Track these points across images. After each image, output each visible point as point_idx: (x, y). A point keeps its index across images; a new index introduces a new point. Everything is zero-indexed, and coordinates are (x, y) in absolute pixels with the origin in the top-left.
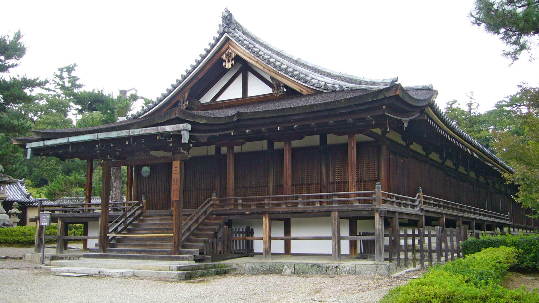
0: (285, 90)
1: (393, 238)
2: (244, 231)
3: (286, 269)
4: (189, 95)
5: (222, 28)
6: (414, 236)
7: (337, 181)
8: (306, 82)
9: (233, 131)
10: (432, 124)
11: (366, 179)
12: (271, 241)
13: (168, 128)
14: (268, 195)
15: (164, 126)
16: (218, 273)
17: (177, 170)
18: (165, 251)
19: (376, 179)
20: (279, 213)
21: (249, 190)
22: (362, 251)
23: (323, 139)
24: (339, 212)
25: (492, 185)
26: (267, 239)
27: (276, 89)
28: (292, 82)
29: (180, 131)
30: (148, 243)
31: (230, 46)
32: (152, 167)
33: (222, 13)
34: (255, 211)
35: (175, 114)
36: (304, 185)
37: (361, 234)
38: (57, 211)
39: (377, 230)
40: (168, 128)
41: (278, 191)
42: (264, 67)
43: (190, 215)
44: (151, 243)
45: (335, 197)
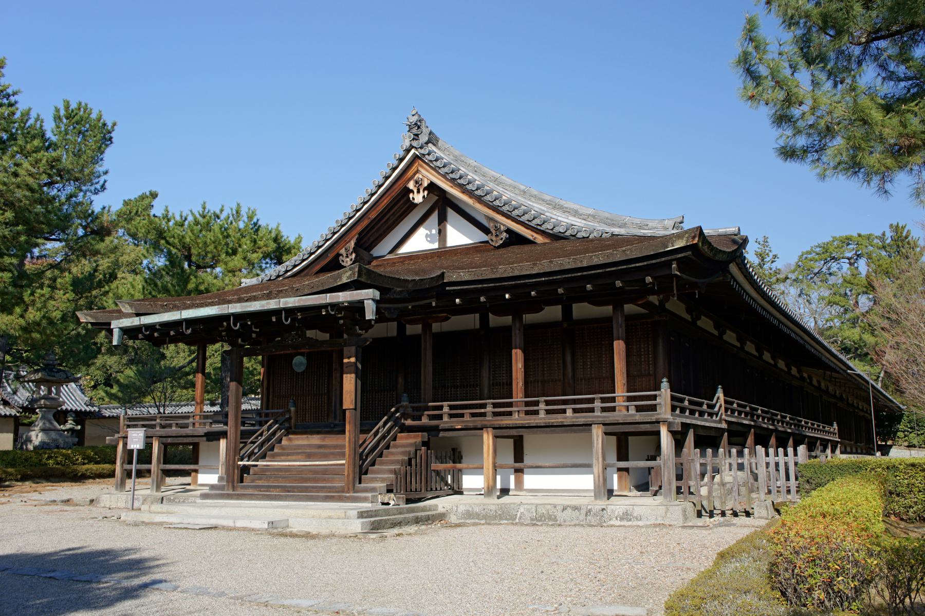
4: (355, 244)
9: (434, 299)
15: (336, 294)
16: (417, 521)
21: (451, 391)
23: (567, 312)
25: (808, 381)
27: (494, 234)
31: (420, 169)
32: (309, 356)
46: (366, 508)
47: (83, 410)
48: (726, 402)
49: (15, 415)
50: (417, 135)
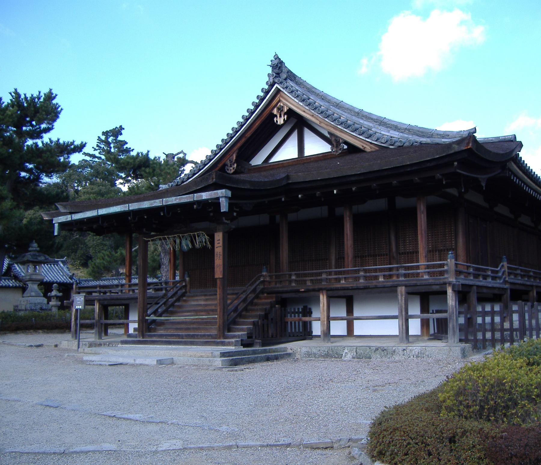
0: (346, 147)
1: (469, 316)
2: (300, 310)
3: (346, 353)
4: (237, 157)
5: (271, 78)
6: (493, 313)
7: (408, 251)
8: (369, 136)
10: (517, 181)
11: (442, 248)
12: (330, 321)
13: (205, 196)
14: (329, 269)
16: (268, 359)
17: (219, 243)
18: (209, 336)
19: (453, 247)
20: (337, 289)
22: (436, 331)
24: (406, 286)
26: (325, 320)
28: (351, 137)
29: (218, 198)
30: (192, 326)
31: (281, 99)
33: (271, 61)
34: (311, 288)
35: (213, 179)
36: (371, 257)
37: (435, 312)
38: (95, 292)
39: (450, 306)
40: (205, 196)
41: (341, 264)
42: (320, 121)
43: (238, 293)
44: (195, 326)
45: (401, 270)
46: (231, 349)
47: (68, 282)
48: (509, 268)
49: (23, 286)
50: (278, 74)
